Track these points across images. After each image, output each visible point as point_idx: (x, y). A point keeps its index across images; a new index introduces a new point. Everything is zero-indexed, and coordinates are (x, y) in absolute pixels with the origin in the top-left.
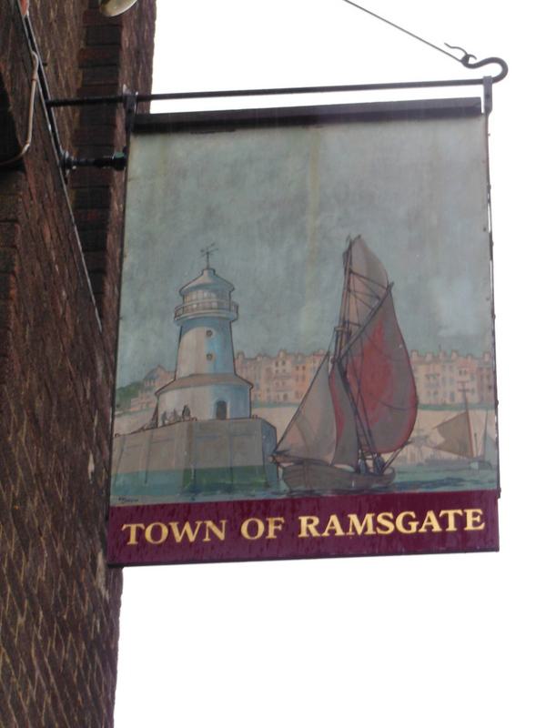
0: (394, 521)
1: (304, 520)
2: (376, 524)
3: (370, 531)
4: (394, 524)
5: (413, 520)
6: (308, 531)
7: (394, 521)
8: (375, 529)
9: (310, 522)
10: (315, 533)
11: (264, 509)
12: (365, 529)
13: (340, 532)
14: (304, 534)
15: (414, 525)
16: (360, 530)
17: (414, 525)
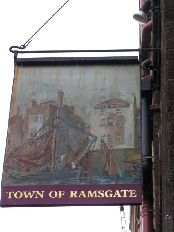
0: (104, 193)
1: (72, 192)
2: (98, 194)
3: (96, 196)
4: (159, 25)
5: (111, 193)
6: (73, 196)
7: (104, 193)
8: (97, 196)
9: (74, 193)
10: (76, 196)
11: (57, 188)
12: (94, 195)
13: (84, 196)
14: (71, 196)
15: (111, 195)
16: (92, 196)
17: (111, 195)
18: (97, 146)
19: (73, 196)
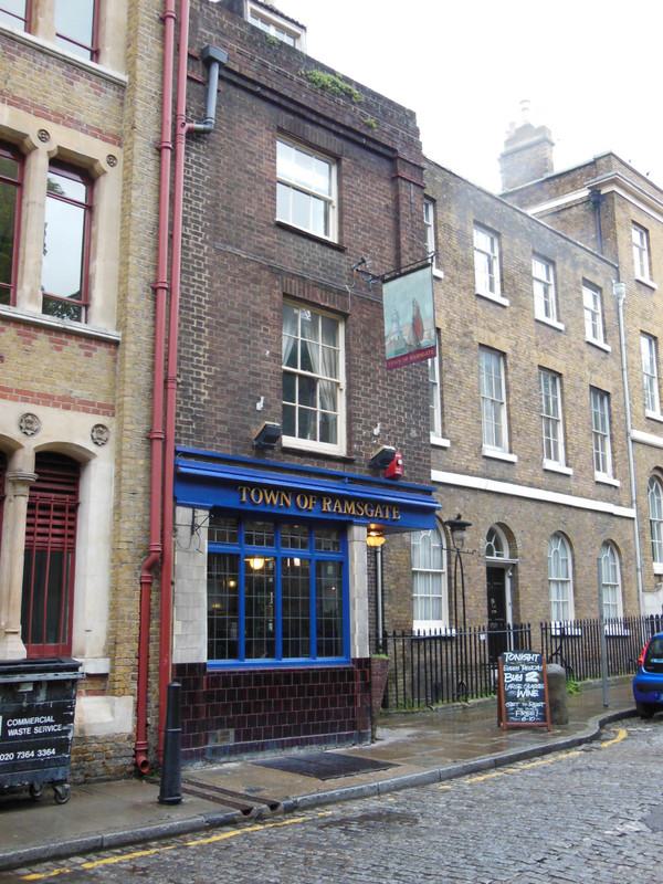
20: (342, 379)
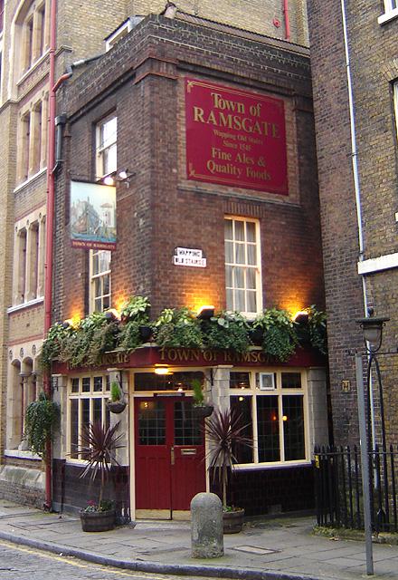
1: (196, 109)
6: (199, 118)
9: (199, 112)
14: (196, 119)
18: (102, 225)
19: (199, 118)
20: (259, 265)
